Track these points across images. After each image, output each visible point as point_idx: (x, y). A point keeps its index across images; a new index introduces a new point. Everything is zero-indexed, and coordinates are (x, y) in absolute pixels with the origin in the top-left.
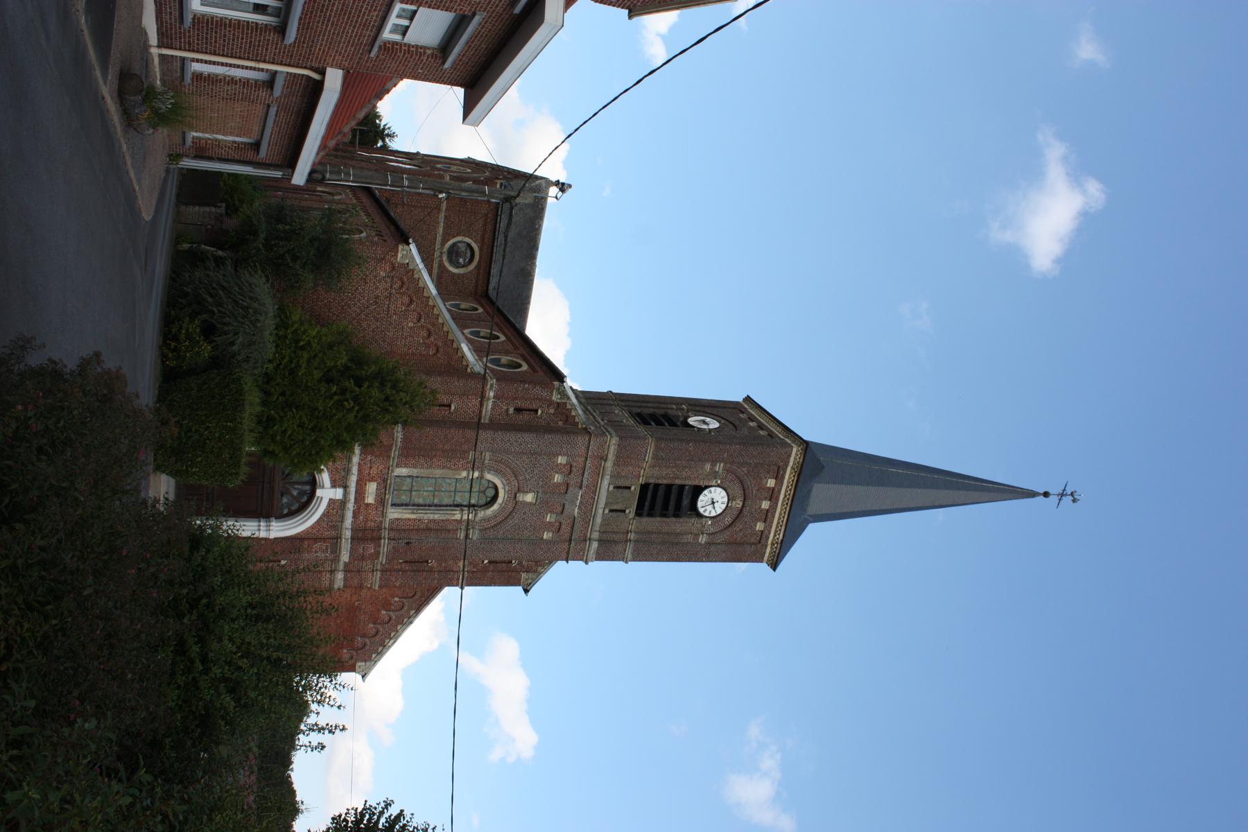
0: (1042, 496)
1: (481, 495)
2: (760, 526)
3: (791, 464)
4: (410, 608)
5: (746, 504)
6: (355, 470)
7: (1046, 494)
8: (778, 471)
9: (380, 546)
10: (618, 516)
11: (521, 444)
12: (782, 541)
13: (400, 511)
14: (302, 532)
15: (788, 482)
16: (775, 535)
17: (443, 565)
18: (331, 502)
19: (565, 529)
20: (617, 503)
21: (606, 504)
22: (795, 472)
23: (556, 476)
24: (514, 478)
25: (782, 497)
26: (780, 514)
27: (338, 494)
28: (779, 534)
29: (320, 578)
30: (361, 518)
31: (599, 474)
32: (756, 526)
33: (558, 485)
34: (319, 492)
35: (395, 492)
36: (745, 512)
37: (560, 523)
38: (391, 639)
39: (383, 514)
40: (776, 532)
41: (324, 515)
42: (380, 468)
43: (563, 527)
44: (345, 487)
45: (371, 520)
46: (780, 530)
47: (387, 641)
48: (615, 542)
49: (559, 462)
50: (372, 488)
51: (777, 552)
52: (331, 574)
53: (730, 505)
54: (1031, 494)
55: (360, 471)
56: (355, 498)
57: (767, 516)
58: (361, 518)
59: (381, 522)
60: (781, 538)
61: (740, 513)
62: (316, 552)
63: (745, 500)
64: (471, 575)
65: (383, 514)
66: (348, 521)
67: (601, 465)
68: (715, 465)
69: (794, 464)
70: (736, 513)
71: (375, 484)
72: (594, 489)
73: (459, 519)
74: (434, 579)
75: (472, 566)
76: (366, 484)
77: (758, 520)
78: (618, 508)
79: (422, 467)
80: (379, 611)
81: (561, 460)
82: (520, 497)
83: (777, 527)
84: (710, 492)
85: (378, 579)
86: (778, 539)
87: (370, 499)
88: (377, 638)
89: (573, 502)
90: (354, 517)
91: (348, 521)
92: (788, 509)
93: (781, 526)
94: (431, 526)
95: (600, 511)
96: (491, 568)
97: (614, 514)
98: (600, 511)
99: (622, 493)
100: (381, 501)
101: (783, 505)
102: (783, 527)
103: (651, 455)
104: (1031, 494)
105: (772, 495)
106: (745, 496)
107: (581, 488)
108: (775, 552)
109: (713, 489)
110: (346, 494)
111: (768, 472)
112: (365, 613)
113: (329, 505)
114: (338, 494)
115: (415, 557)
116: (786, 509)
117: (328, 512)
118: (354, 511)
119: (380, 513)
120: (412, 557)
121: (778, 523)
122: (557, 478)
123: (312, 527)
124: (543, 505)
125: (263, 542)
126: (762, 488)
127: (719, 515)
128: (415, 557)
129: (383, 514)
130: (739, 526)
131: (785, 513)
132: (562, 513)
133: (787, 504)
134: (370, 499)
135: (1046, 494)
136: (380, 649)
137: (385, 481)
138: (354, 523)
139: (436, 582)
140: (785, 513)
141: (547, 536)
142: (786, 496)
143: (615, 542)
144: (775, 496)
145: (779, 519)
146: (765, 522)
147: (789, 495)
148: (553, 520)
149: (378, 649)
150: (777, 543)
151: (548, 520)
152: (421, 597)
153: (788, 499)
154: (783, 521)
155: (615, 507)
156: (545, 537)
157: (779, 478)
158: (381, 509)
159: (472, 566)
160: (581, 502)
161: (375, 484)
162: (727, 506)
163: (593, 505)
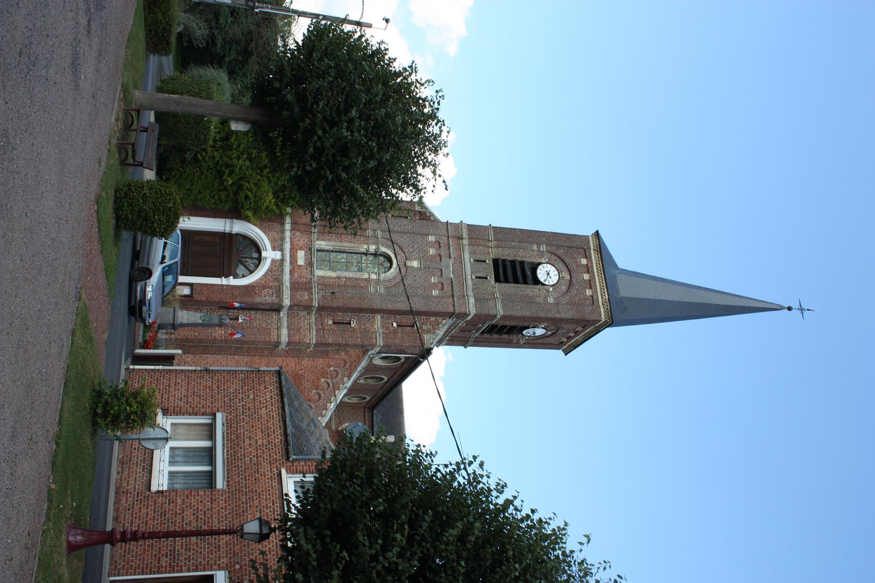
0: (787, 310)
1: (380, 266)
2: (589, 292)
3: (592, 247)
4: (344, 376)
5: (572, 276)
6: (288, 240)
7: (790, 309)
8: (585, 254)
9: (312, 294)
10: (483, 281)
11: (400, 226)
12: (609, 299)
13: (321, 246)
14: (253, 282)
15: (596, 260)
16: (602, 298)
17: (363, 327)
18: (274, 261)
19: (447, 288)
20: (480, 272)
21: (472, 273)
22: (597, 251)
23: (431, 250)
24: (401, 251)
25: (595, 271)
26: (600, 282)
27: (277, 255)
28: (605, 296)
29: (269, 334)
30: (296, 275)
31: (460, 250)
32: (586, 292)
33: (433, 257)
34: (264, 254)
35: (318, 262)
36: (574, 280)
37: (442, 284)
38: (331, 403)
39: (311, 273)
40: (602, 295)
41: (268, 270)
42: (306, 241)
43: (445, 286)
44: (282, 250)
45: (304, 278)
46: (604, 292)
47: (328, 405)
48: (487, 300)
49: (430, 240)
50: (301, 255)
51: (609, 308)
52: (278, 331)
53: (561, 276)
54: (781, 308)
55: (291, 242)
56: (290, 261)
57: (590, 284)
58: (296, 275)
59: (311, 278)
60: (607, 297)
61: (570, 283)
62: (265, 296)
63: (570, 274)
64: (385, 336)
65: (312, 272)
66: (287, 277)
67: (460, 244)
68: (540, 247)
69: (594, 247)
70: (567, 283)
71: (303, 252)
72: (460, 260)
73: (367, 277)
74: (358, 337)
75: (385, 328)
76: (297, 252)
77: (585, 288)
78: (481, 276)
79: (335, 241)
80: (318, 379)
81: (431, 238)
82: (409, 263)
83: (601, 291)
84: (541, 270)
85: (314, 336)
86: (605, 299)
87: (301, 262)
88: (321, 402)
89: (447, 268)
90: (290, 274)
91: (287, 277)
92: (603, 276)
93: (604, 289)
94: (348, 283)
95: (469, 277)
96: (400, 330)
97: (480, 280)
98: (469, 277)
99: (481, 264)
100: (310, 264)
101: (598, 276)
102: (605, 290)
103: (492, 232)
104: (781, 308)
105: (588, 269)
106: (569, 271)
107: (450, 258)
108: (607, 309)
109: (545, 265)
110: (283, 255)
111: (579, 254)
112: (308, 380)
113: (272, 264)
114: (277, 255)
115: (340, 304)
116: (601, 277)
117: (272, 269)
118: (290, 270)
119: (309, 272)
120: (337, 304)
121: (601, 288)
122: (432, 251)
123: (261, 279)
124: (426, 269)
125: (225, 287)
126: (579, 265)
127: (556, 283)
128: (340, 304)
129: (311, 273)
130: (574, 292)
131: (602, 280)
132: (441, 276)
133: (601, 274)
134: (301, 262)
135: (790, 309)
136: (324, 412)
137: (310, 249)
138: (291, 279)
139: (359, 340)
140: (602, 280)
141: (435, 293)
142: (598, 269)
143: (487, 300)
144: (590, 270)
145: (600, 285)
146: (591, 288)
147: (600, 267)
148: (436, 281)
149: (322, 413)
150: (606, 302)
151: (433, 281)
152: (350, 367)
153: (600, 270)
154: (603, 286)
155: (479, 275)
156: (434, 294)
157: (587, 256)
158: (310, 269)
159: (385, 328)
160: (453, 269)
161: (303, 252)
162: (559, 277)
163: (462, 272)
